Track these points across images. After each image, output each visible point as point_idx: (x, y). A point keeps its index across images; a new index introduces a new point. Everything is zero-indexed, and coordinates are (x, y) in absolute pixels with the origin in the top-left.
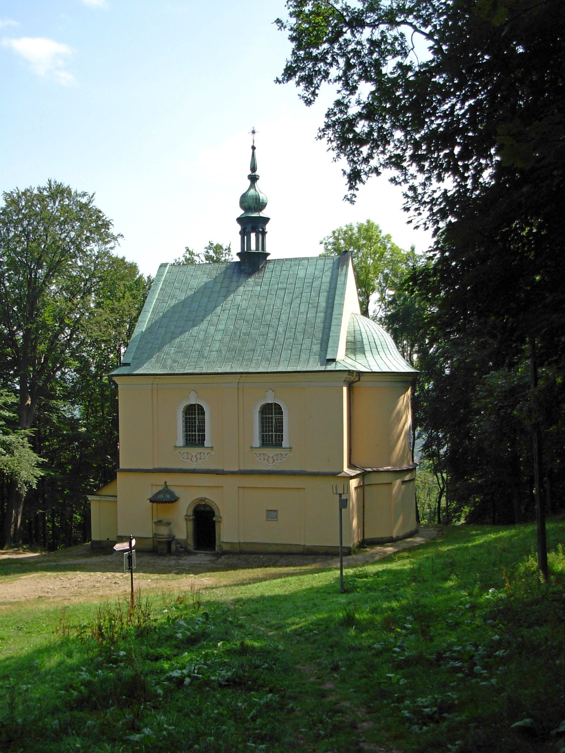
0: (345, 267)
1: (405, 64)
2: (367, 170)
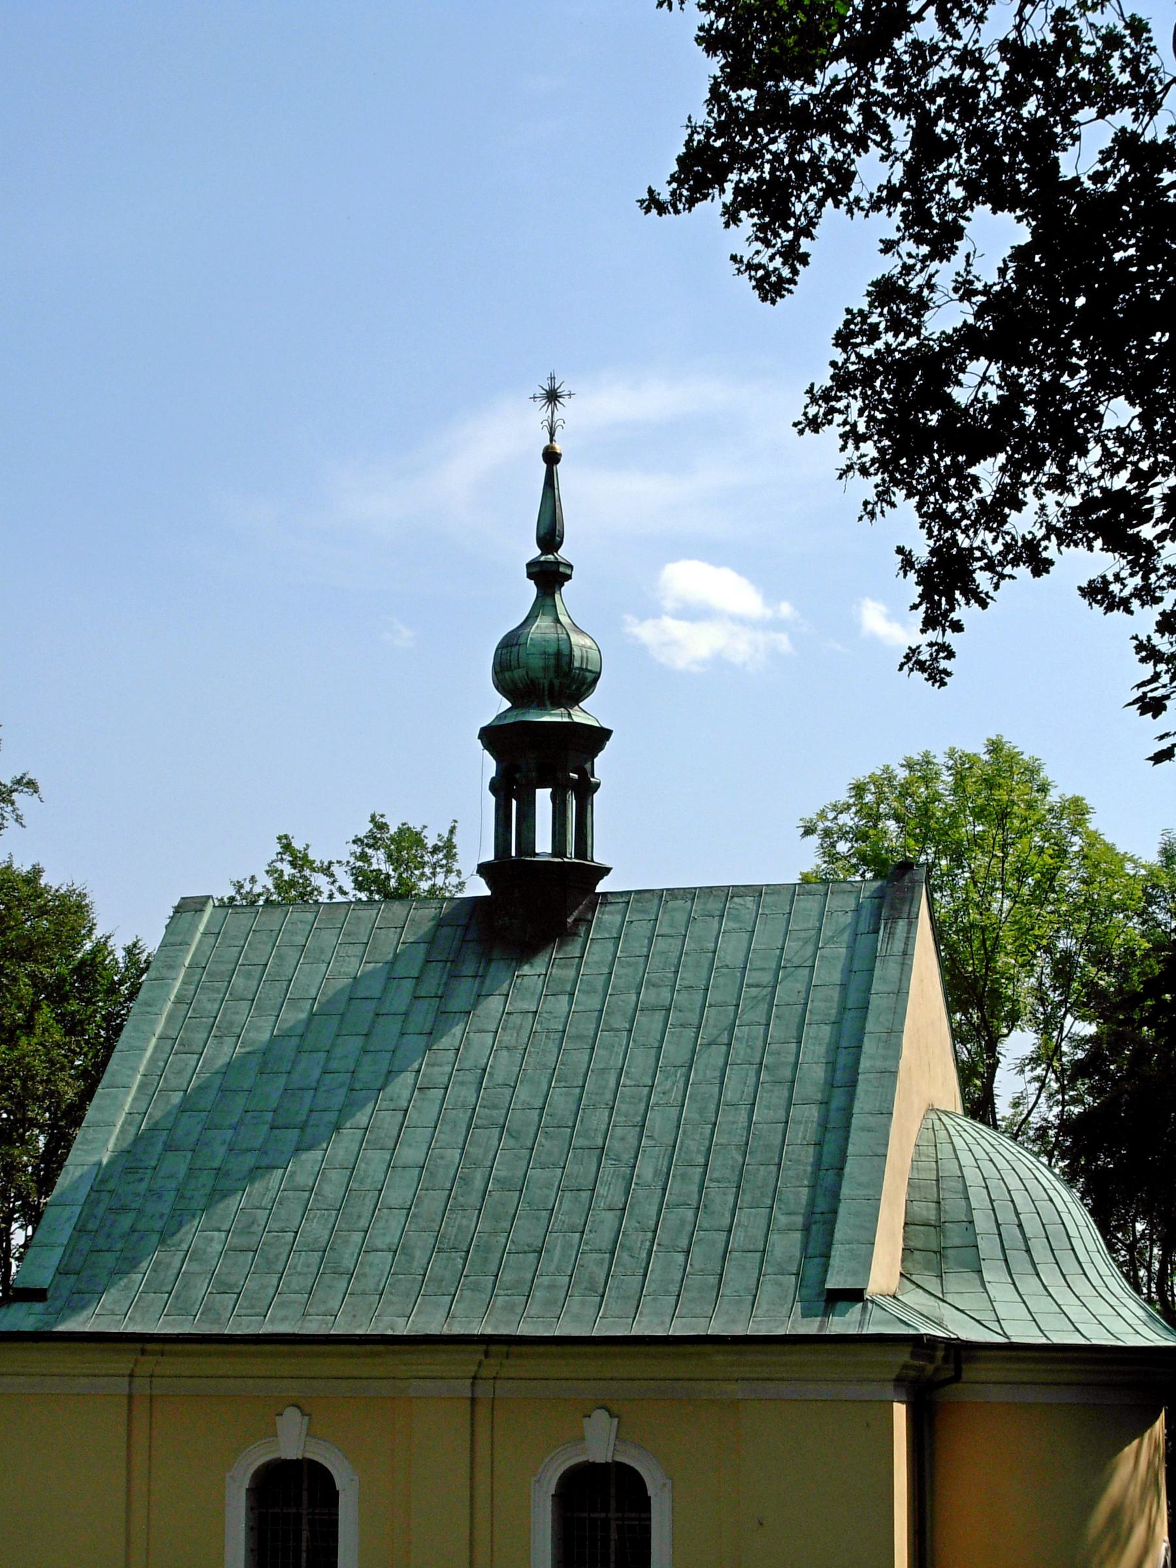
0: (902, 925)
1: (1147, 138)
2: (995, 549)
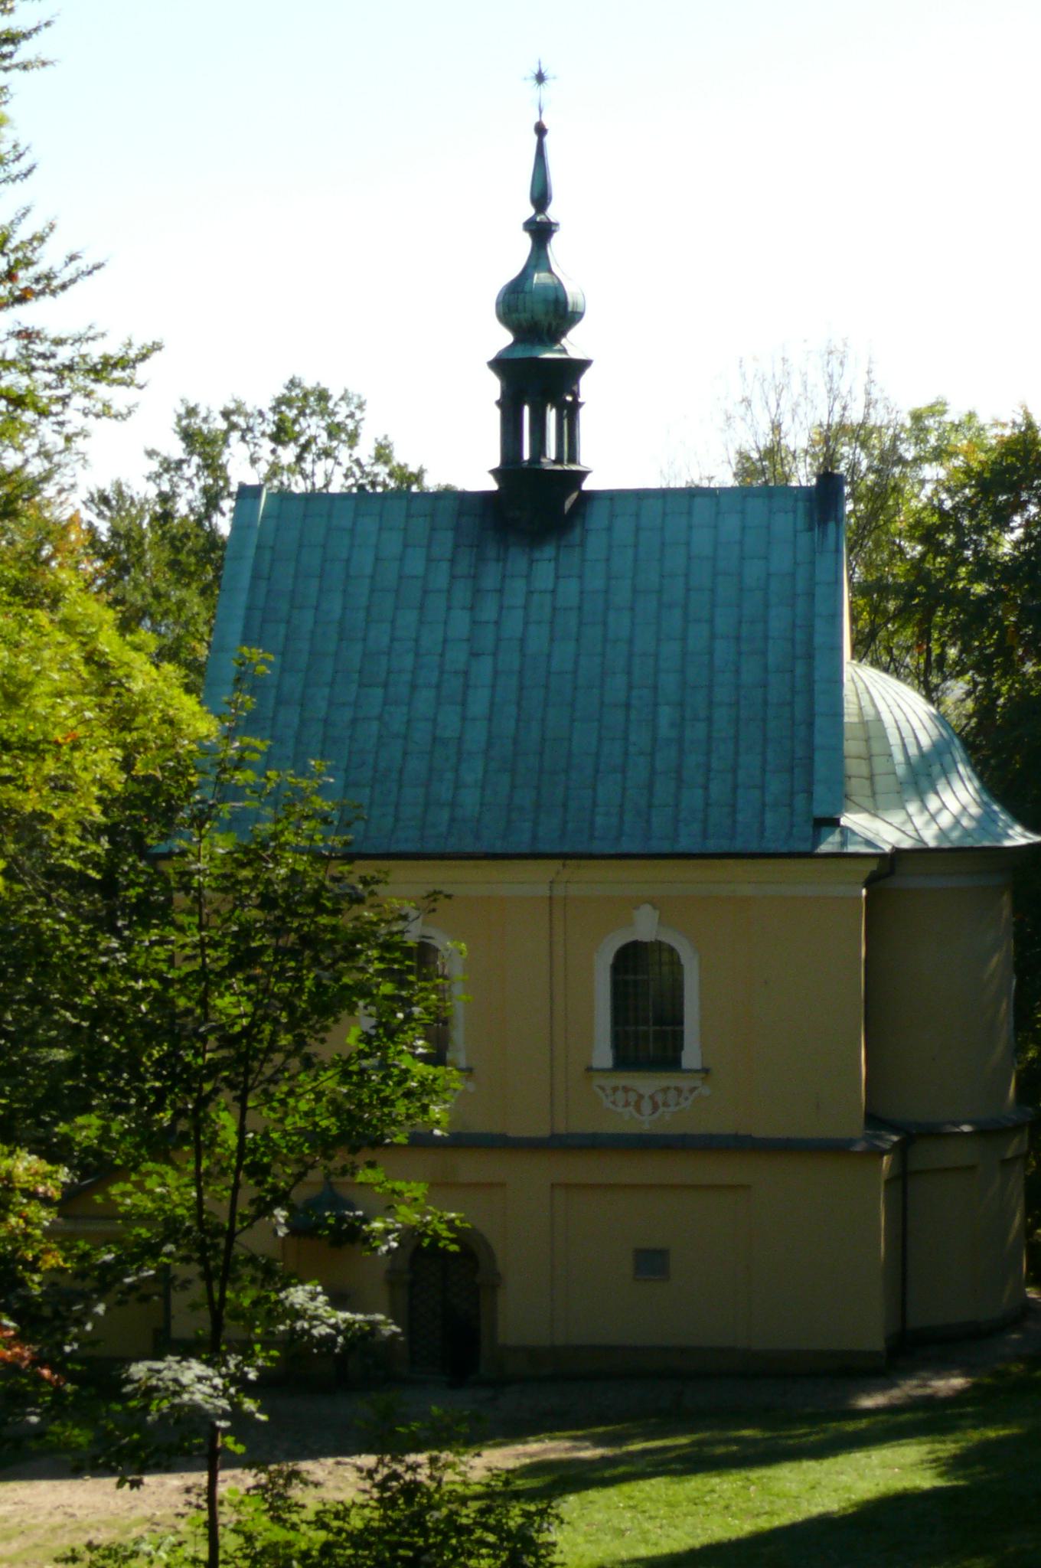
0: (832, 525)
